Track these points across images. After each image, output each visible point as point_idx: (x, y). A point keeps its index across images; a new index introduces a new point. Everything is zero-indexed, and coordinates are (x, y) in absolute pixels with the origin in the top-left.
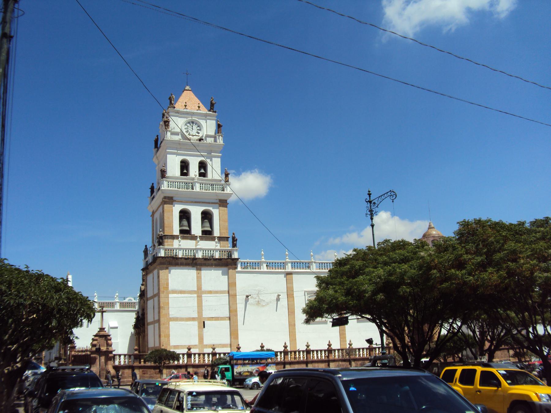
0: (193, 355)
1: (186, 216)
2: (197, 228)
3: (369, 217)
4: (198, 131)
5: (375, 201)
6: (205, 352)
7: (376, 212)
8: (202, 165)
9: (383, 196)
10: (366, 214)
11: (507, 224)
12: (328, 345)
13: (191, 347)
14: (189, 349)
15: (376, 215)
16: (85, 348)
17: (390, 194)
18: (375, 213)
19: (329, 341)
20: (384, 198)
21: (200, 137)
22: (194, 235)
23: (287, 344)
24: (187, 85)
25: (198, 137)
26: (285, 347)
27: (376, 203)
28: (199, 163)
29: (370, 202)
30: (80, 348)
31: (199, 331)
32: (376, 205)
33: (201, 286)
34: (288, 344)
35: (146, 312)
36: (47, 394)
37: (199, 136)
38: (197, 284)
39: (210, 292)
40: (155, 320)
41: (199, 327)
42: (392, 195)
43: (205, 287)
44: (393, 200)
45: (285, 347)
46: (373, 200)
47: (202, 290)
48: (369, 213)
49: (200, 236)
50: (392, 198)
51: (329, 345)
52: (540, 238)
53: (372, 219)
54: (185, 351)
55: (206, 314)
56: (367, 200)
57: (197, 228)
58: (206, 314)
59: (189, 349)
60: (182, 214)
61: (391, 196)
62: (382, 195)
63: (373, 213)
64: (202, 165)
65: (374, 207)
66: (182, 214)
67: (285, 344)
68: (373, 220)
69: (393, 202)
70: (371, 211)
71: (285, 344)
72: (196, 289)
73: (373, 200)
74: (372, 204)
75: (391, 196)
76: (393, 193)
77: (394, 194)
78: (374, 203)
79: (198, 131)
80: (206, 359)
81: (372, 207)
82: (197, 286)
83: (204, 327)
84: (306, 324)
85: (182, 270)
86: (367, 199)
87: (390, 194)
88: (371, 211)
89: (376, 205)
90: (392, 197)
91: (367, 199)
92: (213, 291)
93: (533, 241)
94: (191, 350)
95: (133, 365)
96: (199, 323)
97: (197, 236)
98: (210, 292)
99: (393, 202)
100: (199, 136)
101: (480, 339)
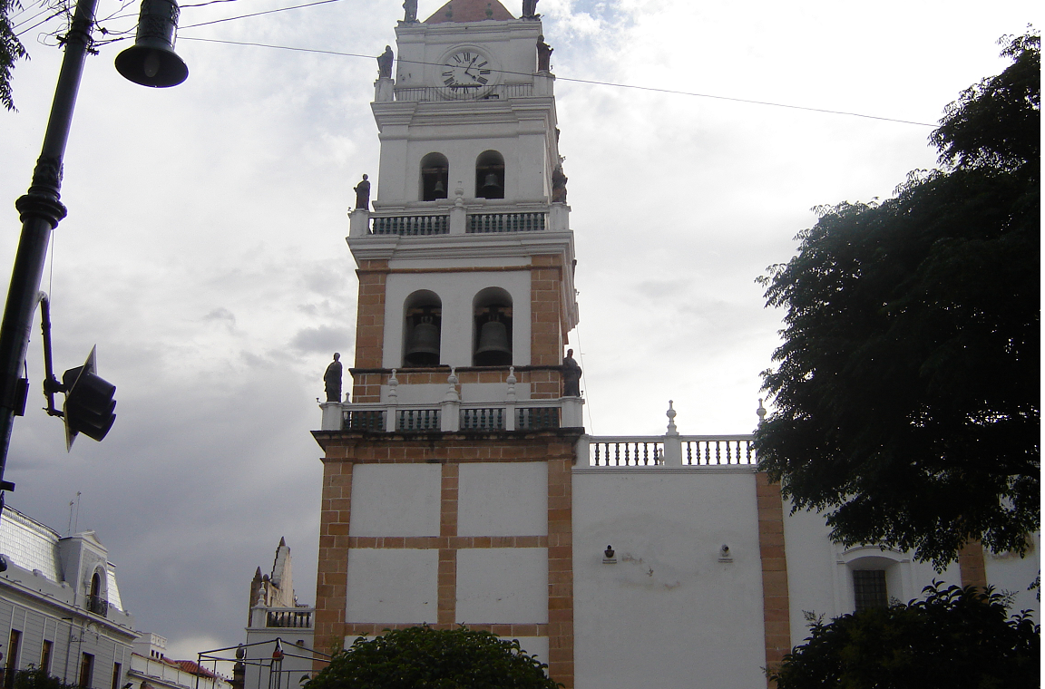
1: (502, 315)
2: (456, 344)
4: (481, 76)
13: (605, 562)
28: (382, 112)
33: (456, 520)
36: (809, 376)
38: (442, 516)
39: (484, 542)
40: (312, 649)
43: (465, 528)
47: (459, 535)
49: (398, 371)
57: (456, 344)
72: (437, 533)
79: (481, 76)
82: (442, 522)
84: (830, 529)
93: (391, 426)
95: (766, 417)
98: (484, 542)
101: (86, 37)
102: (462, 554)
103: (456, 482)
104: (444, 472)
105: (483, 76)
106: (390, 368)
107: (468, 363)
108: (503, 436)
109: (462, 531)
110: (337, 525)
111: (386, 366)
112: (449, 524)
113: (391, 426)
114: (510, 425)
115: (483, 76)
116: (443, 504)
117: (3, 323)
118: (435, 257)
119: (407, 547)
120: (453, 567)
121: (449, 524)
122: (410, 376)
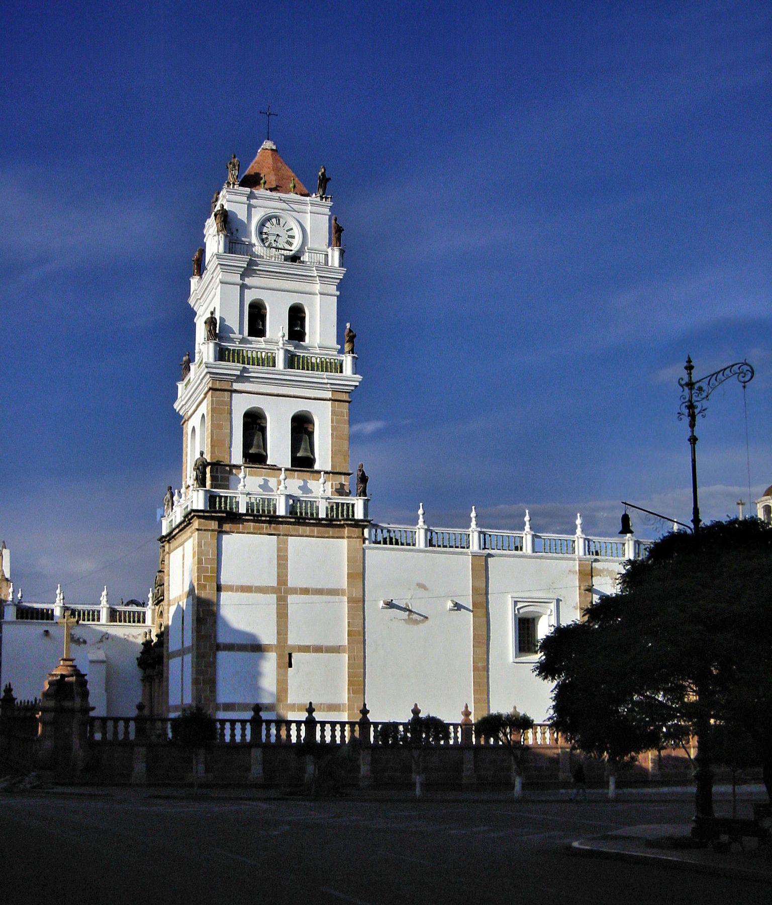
0: (264, 724)
3: (686, 420)
5: (704, 384)
6: (290, 718)
7: (704, 410)
8: (296, 315)
9: (729, 369)
10: (679, 413)
11: (119, 724)
12: (412, 711)
14: (310, 710)
15: (704, 416)
16: (32, 702)
17: (739, 368)
18: (700, 412)
19: (467, 705)
20: (723, 378)
21: (293, 252)
22: (275, 466)
23: (469, 709)
24: (268, 139)
25: (288, 251)
26: (467, 714)
27: (704, 389)
29: (690, 385)
30: (23, 701)
31: (278, 674)
32: (704, 394)
34: (471, 709)
35: (165, 641)
37: (291, 250)
39: (305, 591)
41: (279, 666)
42: (742, 373)
44: (745, 382)
45: (467, 714)
46: (698, 382)
48: (686, 411)
49: (286, 470)
50: (743, 380)
51: (416, 711)
52: (119, 720)
53: (692, 425)
54: (303, 716)
55: (292, 640)
56: (683, 382)
58: (292, 640)
59: (310, 710)
60: (249, 420)
61: (740, 373)
62: (719, 372)
63: (696, 411)
64: (296, 315)
65: (699, 399)
66: (249, 420)
67: (467, 707)
68: (694, 429)
69: (744, 387)
70: (691, 407)
71: (467, 707)
73: (698, 382)
74: (693, 392)
75: (740, 373)
76: (746, 368)
77: (747, 371)
78: (700, 389)
80: (293, 733)
81: (694, 398)
82: (278, 576)
83: (290, 665)
85: (304, 409)
86: (682, 380)
87: (739, 368)
88: (691, 407)
89: (704, 394)
90: (743, 377)
91: (682, 380)
92: (312, 589)
94: (314, 714)
96: (280, 657)
97: (280, 469)
99: (744, 387)
100: (291, 250)
102: (291, 599)
103: (286, 550)
104: (278, 542)
105: (290, 239)
106: (280, 466)
107: (289, 466)
108: (319, 523)
109: (291, 583)
110: (208, 576)
111: (234, 462)
112: (282, 578)
113: (242, 510)
114: (281, 511)
115: (290, 239)
116: (279, 565)
117: (305, 327)
118: (277, 385)
119: (255, 592)
120: (286, 606)
121: (282, 578)
122: (249, 471)
